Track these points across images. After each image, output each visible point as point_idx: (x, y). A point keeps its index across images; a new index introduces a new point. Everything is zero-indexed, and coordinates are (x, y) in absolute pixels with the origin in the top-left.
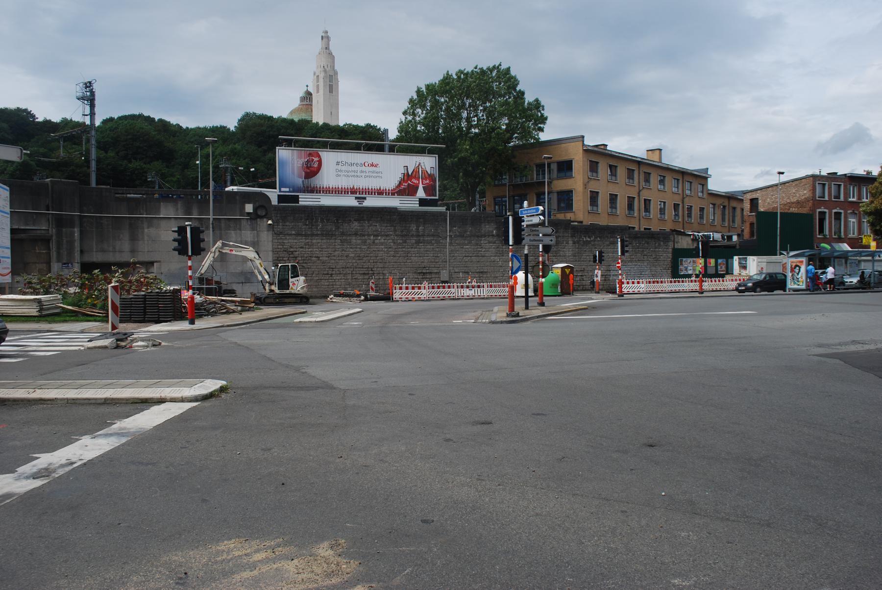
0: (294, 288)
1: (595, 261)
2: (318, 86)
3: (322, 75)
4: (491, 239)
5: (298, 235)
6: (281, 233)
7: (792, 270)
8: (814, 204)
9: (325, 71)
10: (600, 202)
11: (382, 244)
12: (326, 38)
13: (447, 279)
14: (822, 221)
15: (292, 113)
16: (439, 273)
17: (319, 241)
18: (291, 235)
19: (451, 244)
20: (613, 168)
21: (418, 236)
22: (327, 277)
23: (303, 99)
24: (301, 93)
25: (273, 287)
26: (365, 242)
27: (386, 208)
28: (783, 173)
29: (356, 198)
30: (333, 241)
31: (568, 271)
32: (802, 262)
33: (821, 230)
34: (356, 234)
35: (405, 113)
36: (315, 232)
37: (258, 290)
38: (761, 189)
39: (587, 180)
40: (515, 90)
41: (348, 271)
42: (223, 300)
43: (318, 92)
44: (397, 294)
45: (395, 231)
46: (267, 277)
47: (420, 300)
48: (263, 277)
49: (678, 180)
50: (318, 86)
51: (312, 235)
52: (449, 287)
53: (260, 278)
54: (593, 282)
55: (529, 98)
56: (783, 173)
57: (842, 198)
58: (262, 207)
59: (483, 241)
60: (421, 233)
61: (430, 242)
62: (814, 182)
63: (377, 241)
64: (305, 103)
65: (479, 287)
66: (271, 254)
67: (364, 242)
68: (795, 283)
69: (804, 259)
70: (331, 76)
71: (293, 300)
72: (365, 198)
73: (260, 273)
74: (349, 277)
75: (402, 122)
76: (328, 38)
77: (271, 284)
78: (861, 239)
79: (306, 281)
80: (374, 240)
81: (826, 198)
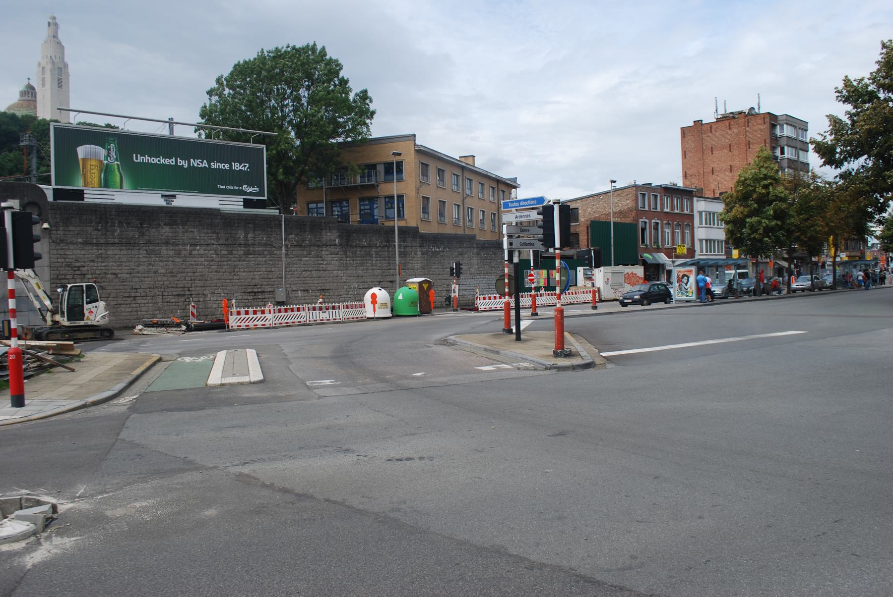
0: (92, 317)
1: (452, 274)
2: (44, 79)
3: (48, 67)
4: (333, 249)
5: (85, 243)
6: (62, 241)
7: (679, 280)
8: (637, 214)
9: (53, 63)
10: (430, 210)
11: (201, 256)
12: (53, 25)
13: (284, 300)
14: (643, 230)
15: (9, 108)
16: (272, 292)
17: (117, 252)
18: (77, 243)
19: (287, 255)
20: (440, 172)
21: (247, 245)
22: (129, 300)
23: (23, 94)
24: (22, 87)
25: (58, 318)
26: (180, 254)
27: (205, 209)
28: (615, 182)
29: (163, 196)
30: (136, 252)
31: (425, 286)
32: (691, 271)
33: (643, 242)
34: (167, 243)
35: (210, 93)
36: (111, 240)
37: (36, 321)
38: (581, 199)
39: (419, 184)
40: (338, 77)
41: (157, 292)
42: (32, 347)
43: (44, 85)
44: (233, 321)
45: (218, 239)
46: (47, 303)
47: (264, 327)
48: (41, 302)
49: (494, 188)
50: (44, 79)
51: (107, 244)
52: (298, 310)
53: (37, 305)
54: (449, 299)
55: (355, 89)
56: (615, 182)
57: (659, 209)
58: (33, 204)
59: (324, 252)
60: (250, 242)
61: (261, 254)
62: (637, 191)
63: (194, 252)
64: (26, 98)
65: (334, 308)
66: (47, 270)
67: (178, 254)
68: (682, 294)
69: (693, 268)
70: (60, 69)
71: (91, 335)
72: (174, 197)
73: (37, 297)
74: (159, 299)
75: (205, 107)
76: (56, 25)
77: (54, 313)
78: (675, 249)
79: (106, 308)
80: (191, 251)
81: (647, 209)
